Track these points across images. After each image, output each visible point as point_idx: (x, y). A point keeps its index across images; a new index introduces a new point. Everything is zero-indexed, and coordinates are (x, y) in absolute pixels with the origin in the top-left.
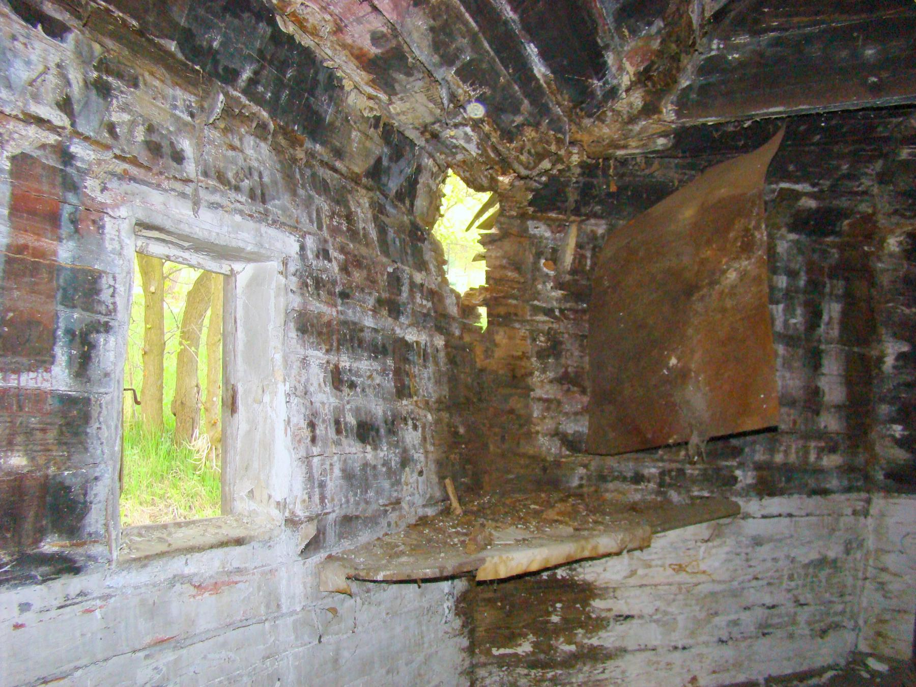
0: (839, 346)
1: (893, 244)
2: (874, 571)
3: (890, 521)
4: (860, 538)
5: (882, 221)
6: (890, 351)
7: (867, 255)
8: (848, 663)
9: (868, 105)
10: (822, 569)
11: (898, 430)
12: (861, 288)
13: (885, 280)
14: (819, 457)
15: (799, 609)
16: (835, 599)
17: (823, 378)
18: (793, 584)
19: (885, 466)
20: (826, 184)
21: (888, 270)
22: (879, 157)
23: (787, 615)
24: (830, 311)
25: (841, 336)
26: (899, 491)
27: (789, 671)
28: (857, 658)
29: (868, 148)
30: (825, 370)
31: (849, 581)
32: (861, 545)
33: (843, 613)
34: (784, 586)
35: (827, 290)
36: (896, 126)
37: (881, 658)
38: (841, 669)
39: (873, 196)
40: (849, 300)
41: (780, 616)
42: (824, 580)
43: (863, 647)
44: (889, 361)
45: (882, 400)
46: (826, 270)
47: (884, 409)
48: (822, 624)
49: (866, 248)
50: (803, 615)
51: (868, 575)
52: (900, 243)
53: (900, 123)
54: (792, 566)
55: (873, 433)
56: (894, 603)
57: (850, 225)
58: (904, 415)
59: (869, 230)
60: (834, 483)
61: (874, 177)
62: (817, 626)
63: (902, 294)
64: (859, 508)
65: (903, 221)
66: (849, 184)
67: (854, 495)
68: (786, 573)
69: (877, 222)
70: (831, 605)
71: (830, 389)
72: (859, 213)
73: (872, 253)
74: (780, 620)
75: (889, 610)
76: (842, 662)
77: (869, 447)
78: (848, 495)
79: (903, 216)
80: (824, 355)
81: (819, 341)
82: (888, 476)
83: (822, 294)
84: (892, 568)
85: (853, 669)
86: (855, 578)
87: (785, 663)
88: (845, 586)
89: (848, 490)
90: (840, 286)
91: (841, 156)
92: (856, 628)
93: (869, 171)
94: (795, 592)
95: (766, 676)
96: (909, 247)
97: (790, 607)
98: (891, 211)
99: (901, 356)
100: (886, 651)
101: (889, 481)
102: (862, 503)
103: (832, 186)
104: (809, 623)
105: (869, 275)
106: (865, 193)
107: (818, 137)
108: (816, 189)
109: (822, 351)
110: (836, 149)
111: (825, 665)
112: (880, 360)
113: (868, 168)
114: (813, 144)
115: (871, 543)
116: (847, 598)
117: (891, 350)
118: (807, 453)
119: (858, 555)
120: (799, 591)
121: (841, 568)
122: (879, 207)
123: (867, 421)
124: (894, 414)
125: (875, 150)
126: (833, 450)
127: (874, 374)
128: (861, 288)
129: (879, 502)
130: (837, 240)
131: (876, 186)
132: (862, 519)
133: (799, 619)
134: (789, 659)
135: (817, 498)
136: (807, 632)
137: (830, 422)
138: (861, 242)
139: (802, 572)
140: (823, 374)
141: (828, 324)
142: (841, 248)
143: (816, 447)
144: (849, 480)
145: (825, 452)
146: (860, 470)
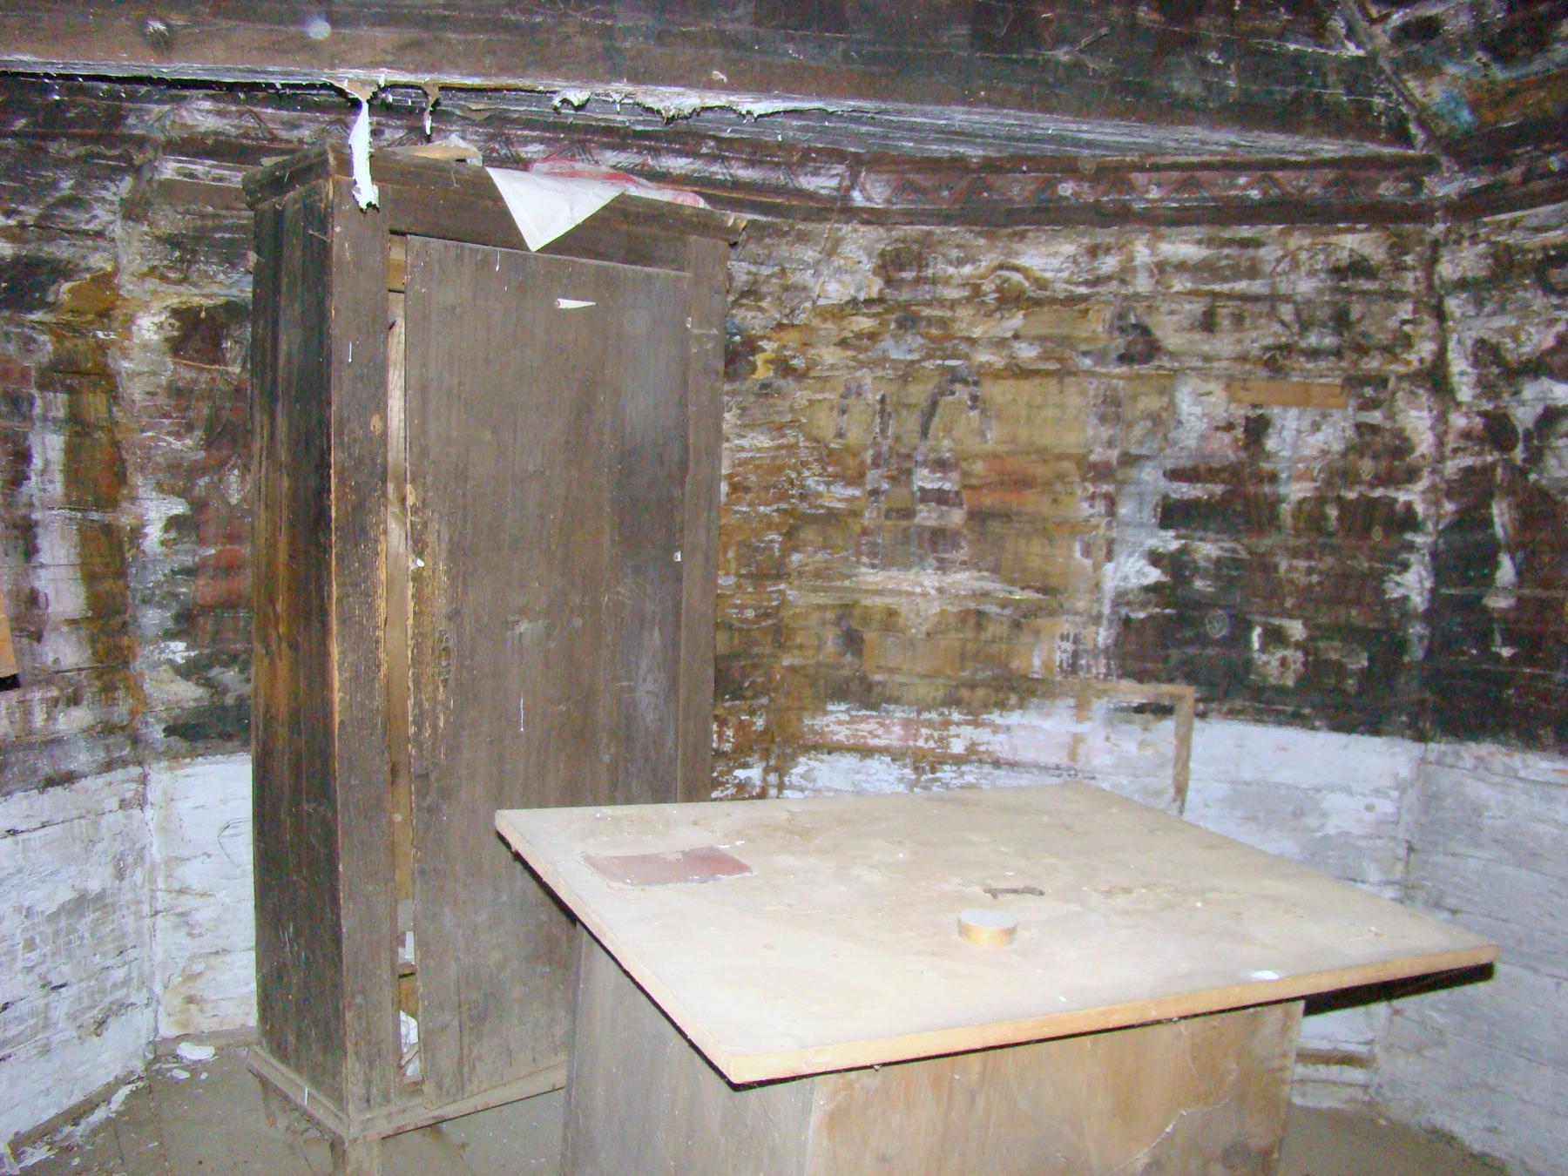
0: (66, 512)
1: (149, 327)
2: (167, 897)
3: (183, 807)
4: (138, 846)
5: (127, 285)
6: (153, 515)
7: (102, 347)
8: (150, 1064)
9: (145, 73)
10: (82, 916)
11: (179, 650)
12: (95, 403)
13: (136, 391)
14: (50, 717)
15: (53, 996)
16: (109, 962)
17: (42, 572)
18: (35, 956)
19: (164, 715)
20: (31, 213)
21: (140, 374)
22: (124, 171)
23: (33, 1014)
24: (45, 449)
25: (67, 495)
26: (193, 754)
27: (52, 1113)
28: (161, 1051)
29: (109, 153)
30: (44, 557)
31: (130, 924)
32: (140, 858)
33: (126, 982)
34: (20, 964)
35: (38, 410)
36: (158, 120)
37: (198, 1039)
38: (140, 1078)
39: (113, 240)
40: (78, 427)
41: (20, 1019)
42: (87, 935)
43: (168, 1030)
44: (154, 534)
45: (146, 601)
46: (33, 373)
47: (153, 618)
48: (95, 1012)
49: (100, 334)
50: (62, 1005)
51: (160, 906)
52: (161, 326)
53: (165, 115)
54: (28, 923)
55: (139, 661)
56: (208, 942)
57: (71, 291)
58: (186, 623)
59: (104, 303)
60: (81, 759)
61: (116, 207)
62: (89, 1018)
63: (167, 415)
64: (129, 795)
65: (164, 287)
66: (68, 212)
67: (119, 774)
68: (20, 939)
69: (119, 287)
70: (105, 974)
71: (57, 591)
72: (88, 269)
73: (113, 342)
74: (22, 1027)
75: (201, 956)
76: (139, 1066)
77: (135, 688)
78: (108, 777)
79: (164, 278)
80: (40, 530)
81: (31, 505)
82: (169, 731)
83: (28, 418)
84: (197, 887)
85: (158, 1071)
86: (140, 916)
87: (41, 1101)
88: (124, 935)
89: (109, 766)
90: (59, 403)
91: (61, 163)
92: (152, 1000)
93: (108, 196)
94: (42, 969)
95: (11, 1137)
96: (176, 333)
97: (37, 999)
98: (145, 269)
99: (173, 523)
100: (207, 1024)
101: (174, 740)
102: (134, 786)
103: (43, 217)
104: (72, 1017)
105: (107, 380)
106: (99, 234)
107: (23, 121)
108: (12, 222)
109: (37, 523)
110: (53, 148)
111: (111, 1079)
112: (137, 533)
113: (105, 188)
114: (14, 135)
115: (156, 852)
116: (132, 954)
117: (155, 511)
118: (28, 713)
119: (139, 875)
120: (49, 964)
121: (113, 905)
122: (124, 261)
123: (125, 641)
124: (170, 624)
125: (118, 158)
126: (74, 700)
127: (129, 557)
128: (95, 403)
129: (161, 777)
130: (49, 318)
131: (119, 223)
132: (136, 812)
133: (54, 1014)
134: (47, 1092)
135: (56, 792)
136: (72, 1032)
137: (65, 652)
138: (92, 323)
139: (48, 929)
140: (42, 566)
141: (43, 472)
142: (59, 332)
143: (42, 700)
144: (107, 748)
145: (61, 706)
146: (123, 728)
